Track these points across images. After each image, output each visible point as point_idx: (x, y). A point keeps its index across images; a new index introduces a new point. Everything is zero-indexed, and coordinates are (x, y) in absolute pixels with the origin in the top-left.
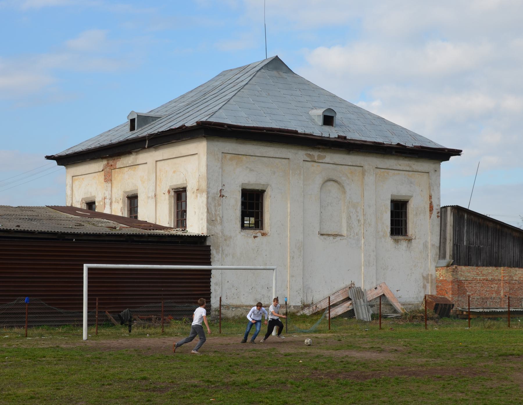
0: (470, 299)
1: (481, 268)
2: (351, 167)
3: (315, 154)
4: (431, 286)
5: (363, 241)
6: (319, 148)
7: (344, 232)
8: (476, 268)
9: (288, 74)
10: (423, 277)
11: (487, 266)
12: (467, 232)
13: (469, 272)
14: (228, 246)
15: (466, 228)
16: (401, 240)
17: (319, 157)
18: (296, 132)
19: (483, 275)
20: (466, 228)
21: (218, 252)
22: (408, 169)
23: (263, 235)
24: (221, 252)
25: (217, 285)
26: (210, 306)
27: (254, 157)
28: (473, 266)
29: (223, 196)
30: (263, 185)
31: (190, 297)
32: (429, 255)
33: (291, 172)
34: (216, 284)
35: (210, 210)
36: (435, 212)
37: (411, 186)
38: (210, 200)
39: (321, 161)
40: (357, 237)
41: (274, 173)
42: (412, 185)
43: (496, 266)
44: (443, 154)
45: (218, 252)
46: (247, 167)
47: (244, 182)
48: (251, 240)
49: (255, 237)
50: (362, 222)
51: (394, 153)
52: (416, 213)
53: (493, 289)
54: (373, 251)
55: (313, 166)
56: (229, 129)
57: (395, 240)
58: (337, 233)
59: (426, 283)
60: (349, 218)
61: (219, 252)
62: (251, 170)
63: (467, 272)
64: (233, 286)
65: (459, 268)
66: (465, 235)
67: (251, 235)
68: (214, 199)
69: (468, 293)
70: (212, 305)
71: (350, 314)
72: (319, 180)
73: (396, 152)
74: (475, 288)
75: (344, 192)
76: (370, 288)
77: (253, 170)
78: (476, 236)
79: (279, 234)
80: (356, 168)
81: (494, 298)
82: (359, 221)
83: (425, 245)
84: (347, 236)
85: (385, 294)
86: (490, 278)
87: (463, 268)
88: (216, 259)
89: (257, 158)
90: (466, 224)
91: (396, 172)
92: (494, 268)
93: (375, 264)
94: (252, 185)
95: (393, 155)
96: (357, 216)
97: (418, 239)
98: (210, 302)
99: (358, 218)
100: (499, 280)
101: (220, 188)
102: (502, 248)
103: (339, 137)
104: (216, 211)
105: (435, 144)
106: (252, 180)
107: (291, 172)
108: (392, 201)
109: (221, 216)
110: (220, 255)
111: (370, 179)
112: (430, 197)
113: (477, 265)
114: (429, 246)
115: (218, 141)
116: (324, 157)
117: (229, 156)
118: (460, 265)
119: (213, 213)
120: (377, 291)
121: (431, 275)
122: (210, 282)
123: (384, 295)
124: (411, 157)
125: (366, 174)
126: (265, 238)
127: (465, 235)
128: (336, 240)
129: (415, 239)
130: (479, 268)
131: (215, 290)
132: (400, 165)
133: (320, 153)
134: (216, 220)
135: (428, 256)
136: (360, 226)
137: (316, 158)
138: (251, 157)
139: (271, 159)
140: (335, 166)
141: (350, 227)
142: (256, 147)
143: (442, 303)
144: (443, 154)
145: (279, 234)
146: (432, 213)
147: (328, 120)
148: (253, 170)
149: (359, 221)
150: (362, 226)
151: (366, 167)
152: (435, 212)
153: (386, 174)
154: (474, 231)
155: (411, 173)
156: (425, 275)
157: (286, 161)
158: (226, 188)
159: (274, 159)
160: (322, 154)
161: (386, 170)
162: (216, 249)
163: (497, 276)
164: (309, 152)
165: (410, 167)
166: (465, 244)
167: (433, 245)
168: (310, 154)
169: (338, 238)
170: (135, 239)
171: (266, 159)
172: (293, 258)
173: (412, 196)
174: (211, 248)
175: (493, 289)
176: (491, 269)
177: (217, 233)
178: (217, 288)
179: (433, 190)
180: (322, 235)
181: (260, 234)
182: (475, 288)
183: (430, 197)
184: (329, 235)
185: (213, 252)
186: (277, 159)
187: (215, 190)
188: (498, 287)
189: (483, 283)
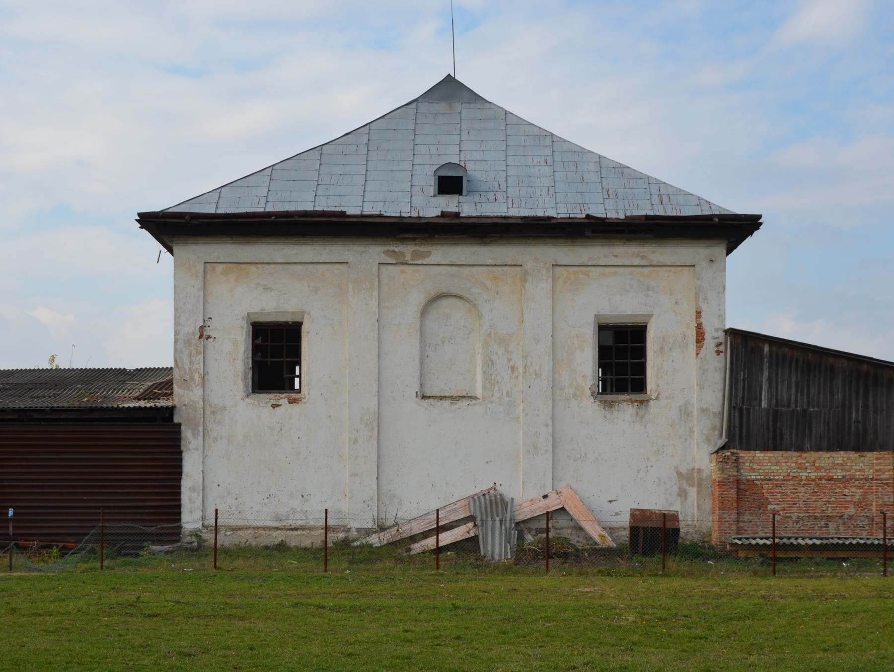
0: (777, 518)
1: (812, 455)
2: (495, 268)
3: (407, 250)
4: (698, 493)
5: (521, 408)
6: (414, 239)
7: (479, 392)
8: (796, 454)
9: (473, 106)
10: (680, 475)
11: (829, 449)
12: (770, 380)
13: (777, 463)
14: (219, 423)
15: (766, 374)
16: (619, 402)
17: (415, 255)
18: (343, 214)
19: (819, 469)
20: (766, 374)
21: (195, 435)
22: (637, 261)
23: (292, 401)
24: (201, 434)
25: (194, 490)
26: (180, 527)
27: (273, 266)
28: (787, 450)
29: (209, 337)
30: (293, 313)
31: (139, 511)
32: (696, 429)
33: (351, 286)
34: (193, 489)
35: (180, 364)
36: (709, 344)
37: (647, 296)
38: (180, 345)
39: (420, 262)
40: (507, 399)
41: (316, 290)
42: (650, 293)
43: (857, 449)
44: (734, 229)
45: (195, 435)
46: (258, 284)
47: (253, 311)
48: (266, 412)
49: (275, 406)
50: (521, 370)
51: (588, 233)
52: (662, 348)
53: (848, 498)
54: (547, 425)
55: (403, 272)
56: (194, 222)
57: (605, 402)
58: (464, 394)
59: (685, 485)
60: (489, 363)
61: (198, 435)
62: (266, 289)
63: (762, 464)
64: (229, 493)
65: (745, 455)
66: (765, 387)
67: (267, 403)
68: (188, 342)
69: (770, 507)
70: (184, 525)
71: (469, 546)
72: (417, 298)
73: (593, 231)
74: (792, 495)
75: (480, 316)
76: (527, 497)
77: (270, 289)
78: (787, 391)
79: (326, 400)
80: (505, 268)
81: (851, 517)
82: (513, 369)
83: (685, 412)
84: (484, 399)
85: (567, 508)
86: (839, 474)
87: (759, 454)
88: (191, 446)
89: (279, 266)
90: (766, 365)
91: (608, 270)
92: (853, 455)
93: (551, 450)
94: (270, 314)
95: (588, 237)
96: (509, 360)
97: (666, 398)
98: (180, 520)
99: (511, 363)
100: (867, 479)
101: (201, 324)
102: (875, 412)
103: (444, 214)
104: (191, 363)
105: (724, 210)
106: (273, 305)
107: (351, 286)
108: (603, 328)
109: (201, 371)
110: (200, 439)
111: (539, 288)
112: (698, 314)
113: (800, 449)
114: (695, 413)
115: (196, 243)
116: (428, 254)
117: (220, 268)
118: (748, 448)
119: (187, 367)
120: (547, 501)
121: (699, 471)
122: (179, 487)
123: (563, 509)
124: (643, 239)
125: (530, 279)
126: (295, 408)
127: (765, 387)
128: (457, 406)
129: (657, 398)
130: (804, 455)
131: (190, 499)
132: (616, 256)
133: (417, 248)
134: (192, 379)
135: (691, 431)
136: (517, 377)
137: (408, 258)
138: (267, 266)
139: (310, 266)
140: (455, 269)
141: (490, 381)
142: (276, 247)
143: (644, 525)
144: (734, 229)
145: (326, 400)
146: (701, 347)
147: (450, 184)
148: (270, 288)
149: (513, 369)
150: (520, 378)
151: (529, 265)
152: (709, 344)
153: (581, 276)
154: (790, 378)
155: (647, 270)
156: (684, 471)
157: (345, 265)
158: (213, 324)
159: (316, 266)
160: (422, 249)
161: (582, 269)
162: (193, 430)
163: (860, 470)
164: (392, 248)
165: (643, 257)
166: (764, 404)
167: (704, 411)
168: (394, 252)
169: (463, 403)
170: (35, 416)
171: (299, 267)
172: (356, 441)
173: (650, 316)
174: (183, 428)
175: (848, 498)
176: (840, 457)
177: (194, 402)
178: (194, 495)
179: (705, 299)
180: (424, 397)
181: (286, 401)
182: (792, 495)
183: (698, 314)
184: (442, 398)
185: (187, 433)
186: (322, 265)
187: (192, 326)
188: (864, 495)
189: (818, 485)
